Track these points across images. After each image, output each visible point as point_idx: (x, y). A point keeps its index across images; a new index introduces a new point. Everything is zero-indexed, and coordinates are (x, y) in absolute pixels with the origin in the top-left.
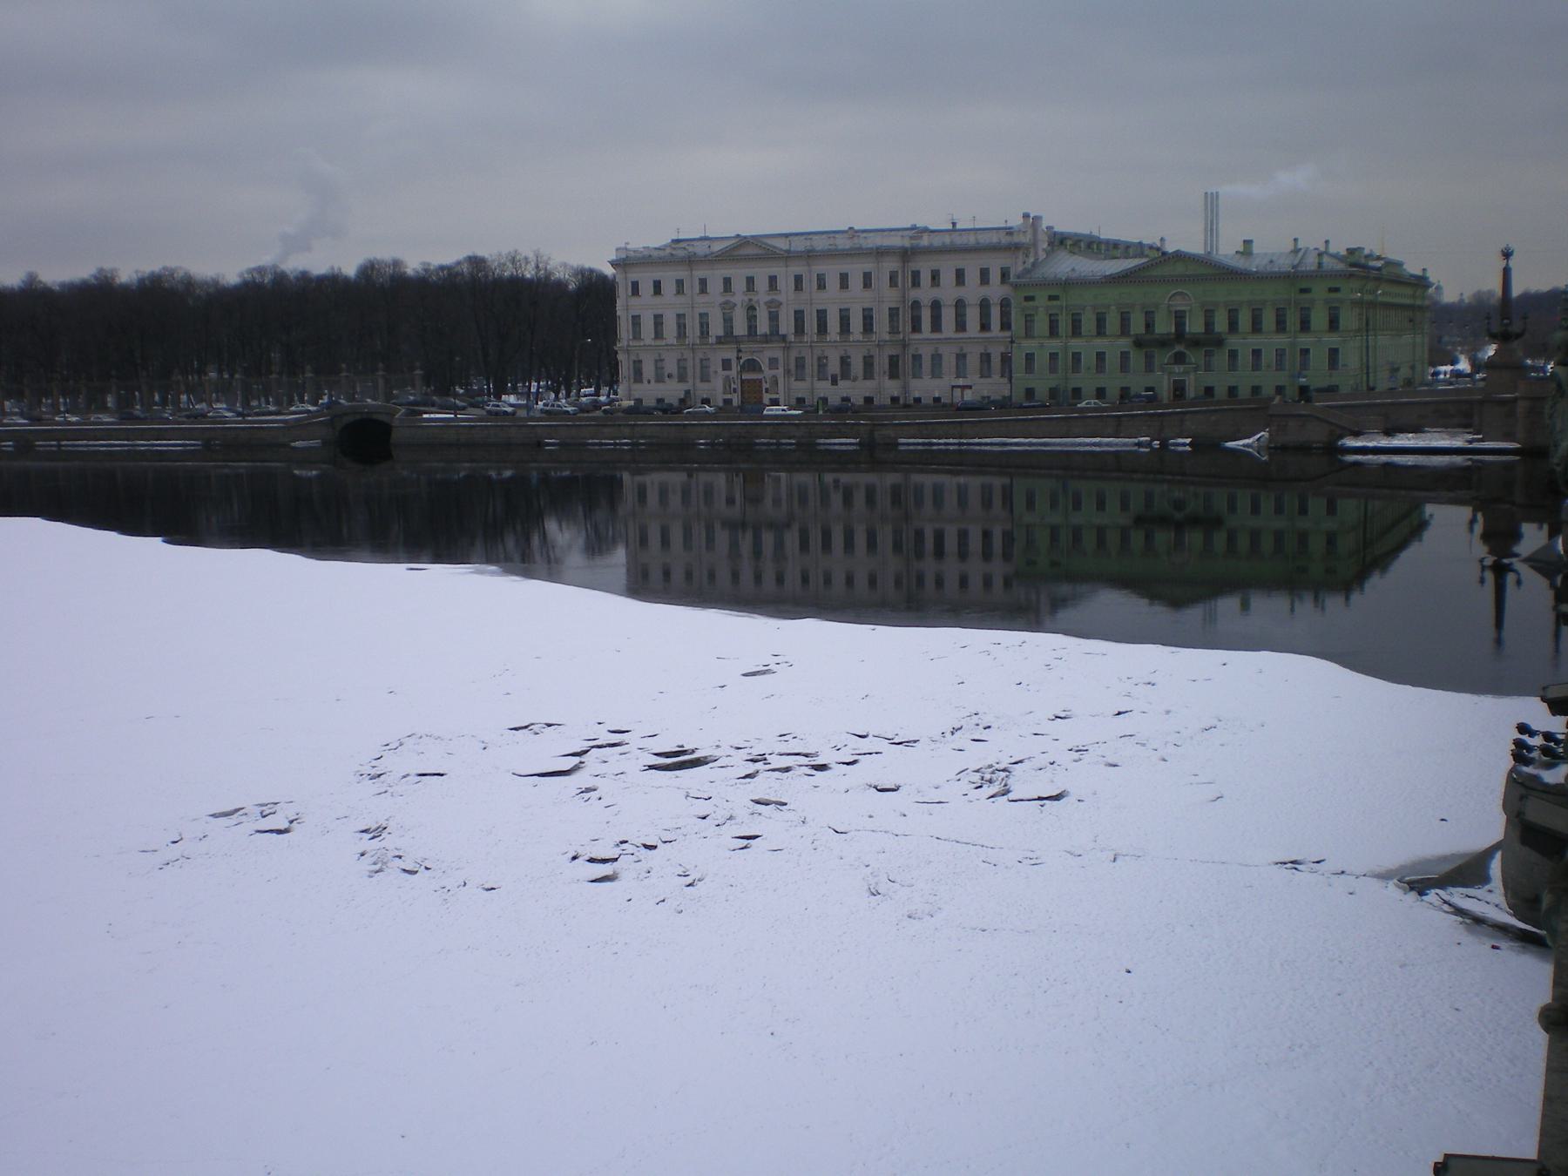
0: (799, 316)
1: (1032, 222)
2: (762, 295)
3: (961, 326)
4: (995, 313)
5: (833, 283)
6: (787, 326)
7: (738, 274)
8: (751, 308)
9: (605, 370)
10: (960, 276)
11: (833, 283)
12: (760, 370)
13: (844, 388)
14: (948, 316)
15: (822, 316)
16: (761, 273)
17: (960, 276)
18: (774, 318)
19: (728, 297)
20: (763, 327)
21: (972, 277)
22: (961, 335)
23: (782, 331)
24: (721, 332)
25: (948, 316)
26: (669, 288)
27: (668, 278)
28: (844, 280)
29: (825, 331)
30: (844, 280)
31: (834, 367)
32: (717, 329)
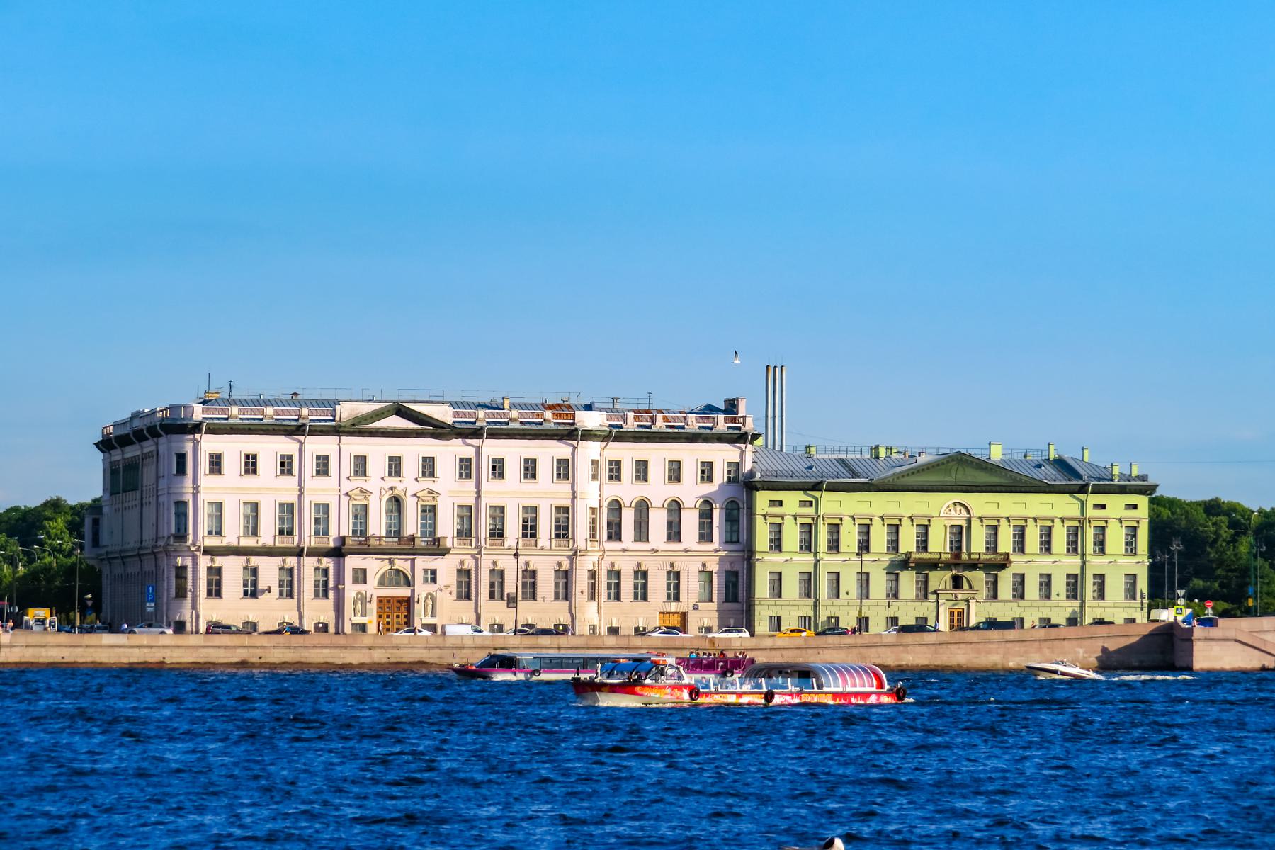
3: (674, 533)
5: (513, 469)
10: (675, 473)
11: (513, 469)
12: (409, 583)
13: (529, 613)
14: (658, 520)
16: (412, 450)
17: (675, 473)
18: (429, 512)
20: (412, 526)
21: (690, 472)
25: (658, 520)
27: (269, 448)
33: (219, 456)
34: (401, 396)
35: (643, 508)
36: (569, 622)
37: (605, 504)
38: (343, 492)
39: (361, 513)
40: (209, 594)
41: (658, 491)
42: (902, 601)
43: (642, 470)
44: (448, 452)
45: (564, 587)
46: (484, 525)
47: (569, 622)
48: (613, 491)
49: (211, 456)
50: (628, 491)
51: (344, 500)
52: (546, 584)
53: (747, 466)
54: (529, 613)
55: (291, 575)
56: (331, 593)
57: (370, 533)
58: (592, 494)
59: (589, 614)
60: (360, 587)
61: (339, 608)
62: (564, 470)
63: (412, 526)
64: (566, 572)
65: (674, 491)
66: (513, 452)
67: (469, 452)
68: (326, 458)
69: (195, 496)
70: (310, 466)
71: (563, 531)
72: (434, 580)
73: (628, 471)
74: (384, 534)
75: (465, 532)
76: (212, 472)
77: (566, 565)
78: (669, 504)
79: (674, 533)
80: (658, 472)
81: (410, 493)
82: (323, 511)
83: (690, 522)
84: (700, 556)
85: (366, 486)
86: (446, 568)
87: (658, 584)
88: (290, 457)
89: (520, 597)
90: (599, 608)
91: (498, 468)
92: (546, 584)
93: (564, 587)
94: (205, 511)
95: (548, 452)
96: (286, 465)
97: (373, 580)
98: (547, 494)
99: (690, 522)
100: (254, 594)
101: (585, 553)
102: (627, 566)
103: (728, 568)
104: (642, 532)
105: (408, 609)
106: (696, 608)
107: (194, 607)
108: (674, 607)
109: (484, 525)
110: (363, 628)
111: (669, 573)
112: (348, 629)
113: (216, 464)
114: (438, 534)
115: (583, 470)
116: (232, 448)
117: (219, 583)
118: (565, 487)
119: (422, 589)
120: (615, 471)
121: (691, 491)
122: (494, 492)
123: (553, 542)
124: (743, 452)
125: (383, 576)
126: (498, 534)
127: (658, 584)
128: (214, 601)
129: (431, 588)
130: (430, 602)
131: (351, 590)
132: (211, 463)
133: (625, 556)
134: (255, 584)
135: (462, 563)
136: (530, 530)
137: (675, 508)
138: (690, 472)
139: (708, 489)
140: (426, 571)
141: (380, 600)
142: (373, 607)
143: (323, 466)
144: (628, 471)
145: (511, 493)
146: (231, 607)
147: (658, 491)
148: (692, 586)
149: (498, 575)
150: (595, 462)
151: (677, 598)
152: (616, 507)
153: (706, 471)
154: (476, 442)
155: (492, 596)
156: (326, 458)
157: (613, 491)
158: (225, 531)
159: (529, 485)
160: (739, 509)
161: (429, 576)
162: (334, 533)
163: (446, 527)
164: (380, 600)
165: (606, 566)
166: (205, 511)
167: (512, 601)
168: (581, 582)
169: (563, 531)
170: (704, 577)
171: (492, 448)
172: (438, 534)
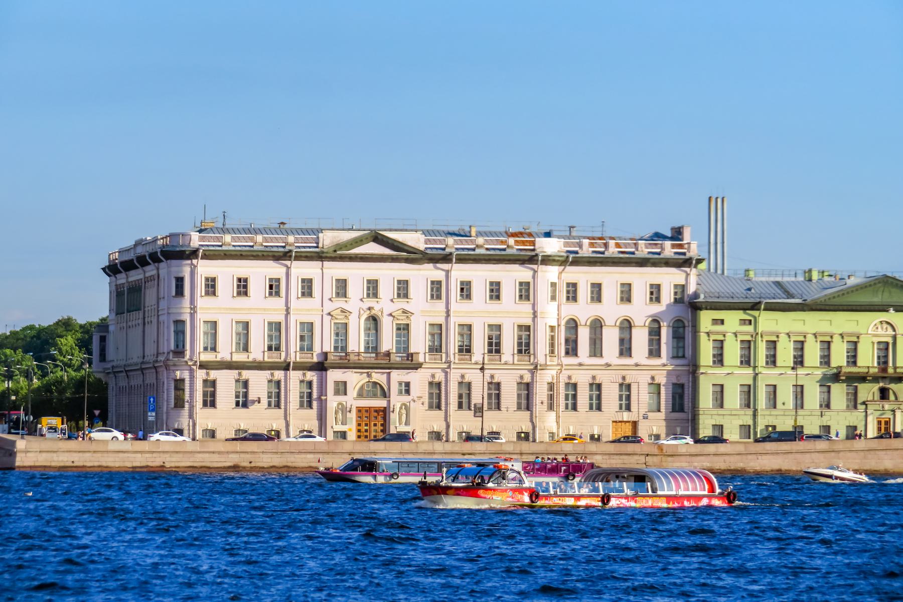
3: (626, 349)
5: (480, 291)
8: (374, 321)
10: (626, 295)
11: (480, 291)
12: (385, 395)
13: (492, 421)
14: (611, 338)
15: (467, 330)
16: (388, 274)
17: (626, 295)
18: (404, 330)
19: (371, 302)
20: (388, 342)
21: (640, 293)
25: (611, 338)
27: (260, 273)
31: (478, 395)
35: (597, 326)
36: (530, 430)
37: (563, 323)
38: (326, 312)
39: (342, 331)
40: (205, 404)
43: (597, 292)
44: (421, 276)
45: (526, 401)
46: (453, 342)
47: (530, 430)
48: (570, 310)
50: (584, 311)
51: (327, 319)
52: (509, 395)
53: (692, 289)
57: (350, 349)
58: (551, 314)
60: (341, 398)
62: (525, 292)
63: (388, 342)
64: (528, 384)
65: (626, 310)
70: (296, 288)
71: (525, 347)
72: (408, 392)
73: (584, 292)
74: (362, 350)
75: (436, 349)
76: (207, 293)
77: (527, 378)
78: (622, 323)
79: (626, 349)
80: (610, 293)
81: (386, 312)
82: (308, 328)
83: (640, 339)
86: (419, 380)
87: (611, 395)
90: (558, 417)
91: (466, 290)
92: (509, 395)
93: (526, 401)
94: (201, 329)
95: (511, 276)
96: (274, 288)
97: (352, 392)
98: (510, 314)
100: (245, 405)
101: (545, 367)
102: (582, 379)
103: (675, 381)
104: (596, 349)
105: (384, 418)
108: (626, 416)
109: (453, 342)
111: (621, 385)
113: (211, 286)
114: (412, 350)
115: (542, 292)
116: (225, 272)
118: (526, 307)
119: (397, 401)
120: (572, 293)
121: (641, 311)
122: (461, 311)
123: (516, 357)
124: (688, 275)
125: (362, 387)
126: (466, 349)
127: (611, 395)
128: (209, 411)
129: (405, 399)
130: (404, 411)
132: (207, 286)
133: (582, 370)
134: (246, 395)
135: (433, 376)
136: (495, 347)
138: (640, 293)
140: (400, 384)
141: (359, 410)
142: (353, 416)
144: (584, 292)
145: (478, 313)
147: (611, 310)
148: (642, 397)
149: (466, 386)
150: (553, 285)
151: (628, 408)
152: (573, 325)
153: (655, 293)
156: (310, 281)
157: (570, 310)
159: (494, 306)
160: (684, 327)
161: (403, 388)
162: (317, 349)
163: (419, 343)
164: (359, 410)
165: (563, 379)
166: (201, 329)
167: (479, 411)
168: (541, 393)
169: (525, 347)
171: (460, 272)
172: (412, 350)
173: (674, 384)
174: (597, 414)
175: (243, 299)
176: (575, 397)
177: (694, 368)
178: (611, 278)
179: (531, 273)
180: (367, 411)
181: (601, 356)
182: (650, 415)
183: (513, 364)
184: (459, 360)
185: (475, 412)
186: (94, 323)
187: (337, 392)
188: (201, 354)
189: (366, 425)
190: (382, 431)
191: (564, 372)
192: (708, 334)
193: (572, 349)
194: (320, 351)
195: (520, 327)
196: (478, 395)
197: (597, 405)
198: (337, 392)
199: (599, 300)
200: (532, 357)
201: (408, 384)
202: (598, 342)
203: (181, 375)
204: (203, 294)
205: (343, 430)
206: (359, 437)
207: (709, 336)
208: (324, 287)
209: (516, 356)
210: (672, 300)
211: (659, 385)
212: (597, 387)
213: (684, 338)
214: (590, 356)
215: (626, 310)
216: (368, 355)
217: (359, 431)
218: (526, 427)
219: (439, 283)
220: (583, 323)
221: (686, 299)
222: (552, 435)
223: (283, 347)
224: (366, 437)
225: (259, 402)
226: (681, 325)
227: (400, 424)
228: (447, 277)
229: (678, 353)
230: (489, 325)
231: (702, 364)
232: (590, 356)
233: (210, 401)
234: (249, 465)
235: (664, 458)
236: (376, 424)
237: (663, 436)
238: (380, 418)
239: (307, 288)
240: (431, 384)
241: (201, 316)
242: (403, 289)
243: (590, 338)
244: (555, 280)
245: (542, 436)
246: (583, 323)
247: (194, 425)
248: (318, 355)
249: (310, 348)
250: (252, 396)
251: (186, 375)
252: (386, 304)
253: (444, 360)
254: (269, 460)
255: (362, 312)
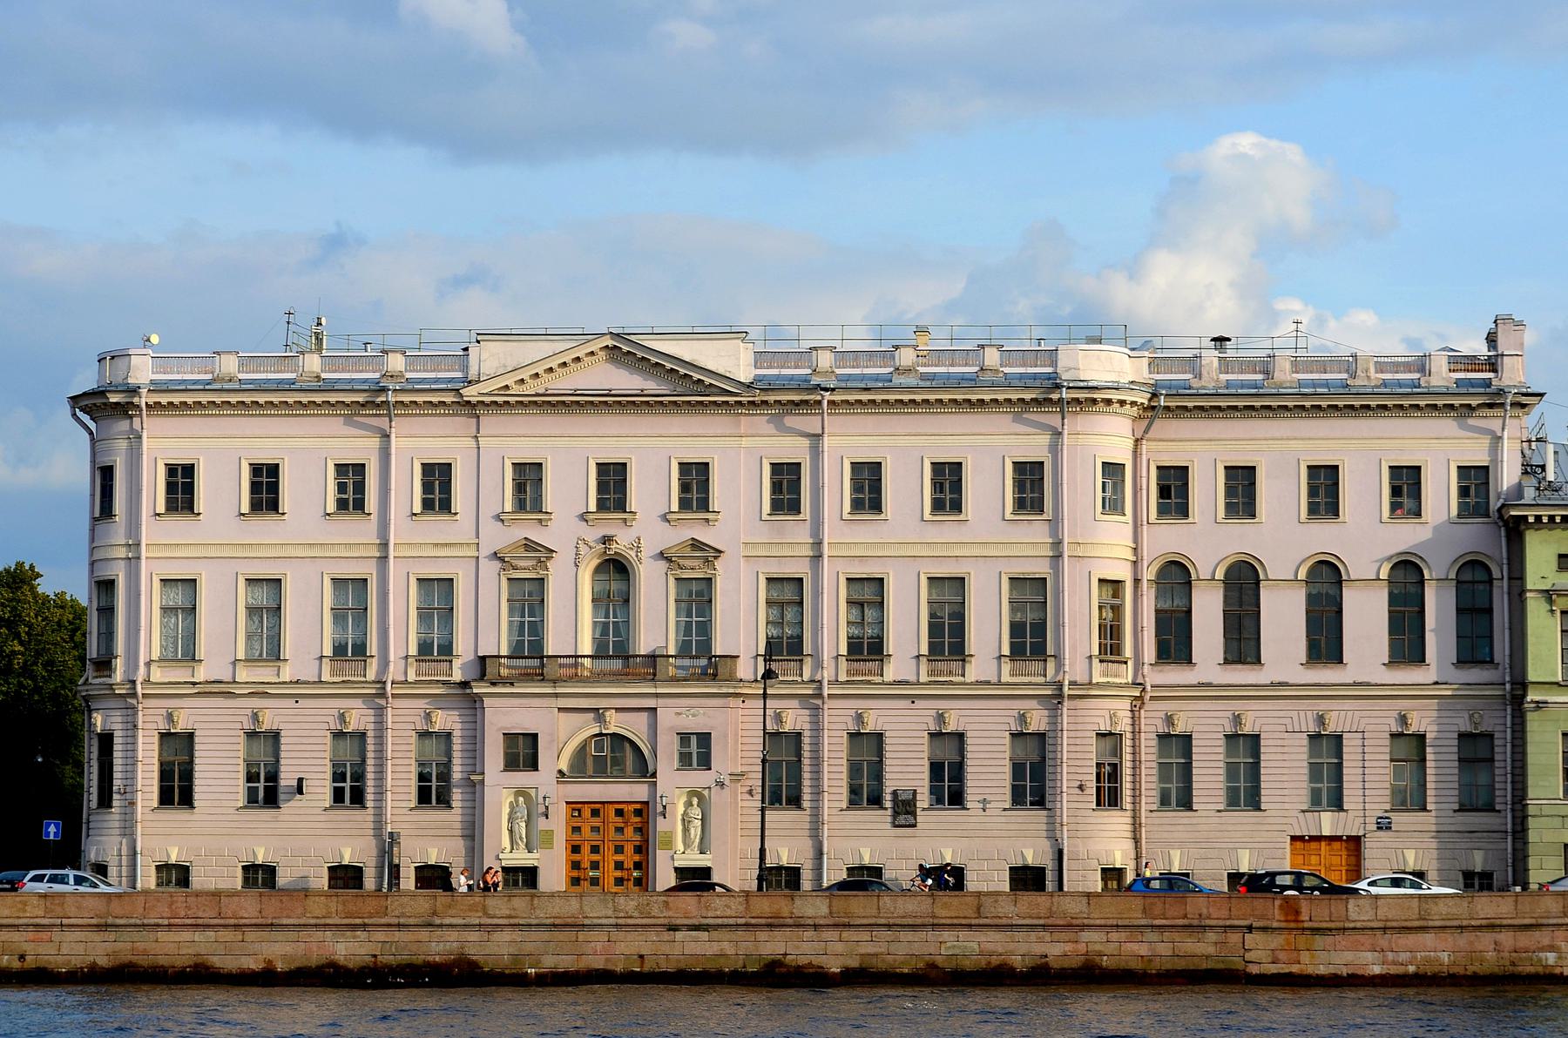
0: (787, 595)
1: (20, 565)
2: (649, 526)
3: (1325, 640)
4: (1438, 608)
5: (906, 489)
6: (740, 628)
7: (569, 455)
8: (616, 568)
9: (1043, 869)
10: (1324, 490)
11: (906, 489)
12: (645, 770)
13: (940, 838)
14: (1283, 617)
15: (868, 595)
16: (653, 451)
17: (1324, 490)
18: (697, 599)
19: (609, 525)
20: (655, 626)
21: (1364, 491)
22: (1326, 674)
23: (554, 644)
24: (496, 640)
25: (1283, 617)
26: (307, 490)
27: (309, 453)
28: (948, 485)
29: (958, 651)
30: (948, 485)
31: (907, 770)
32: (484, 627)
33: (189, 470)
34: (634, 318)
35: (1243, 582)
36: (1048, 862)
37: (1149, 574)
38: (485, 551)
39: (529, 600)
40: (166, 799)
41: (1282, 539)
42: (543, 895)
43: (1242, 488)
44: (741, 456)
45: (1032, 784)
46: (831, 628)
47: (1048, 862)
48: (1167, 539)
49: (172, 470)
50: (1207, 540)
51: (490, 569)
52: (989, 772)
53: (1508, 475)
54: (940, 838)
55: (1117, 751)
56: (457, 796)
57: (550, 650)
58: (1109, 547)
59: (1104, 841)
60: (522, 778)
61: (473, 833)
62: (1031, 486)
63: (655, 626)
64: (1041, 736)
65: (1324, 538)
66: (906, 449)
67: (791, 449)
68: (446, 469)
69: (133, 561)
70: (407, 489)
71: (1030, 639)
72: (705, 762)
73: (1207, 491)
74: (586, 648)
75: (785, 648)
76: (172, 507)
77: (1038, 721)
78: (1311, 571)
79: (1325, 640)
80: (1280, 493)
81: (649, 548)
82: (438, 595)
83: (1366, 617)
84: (1386, 691)
85: (537, 535)
86: (739, 734)
87: (1287, 771)
88: (360, 469)
89: (923, 800)
90: (1136, 826)
91: (868, 487)
92: (989, 772)
93: (1032, 784)
94: (152, 601)
95: (989, 449)
96: (351, 488)
97: (555, 757)
98: (989, 545)
99: (1366, 617)
100: (271, 799)
101: (1086, 691)
102: (1207, 727)
103: (1466, 726)
104: (1243, 640)
105: (642, 830)
106: (1384, 825)
107: (128, 830)
108: (1328, 823)
109: (831, 628)
110: (529, 876)
111: (1315, 738)
112: (665, 878)
113: (181, 487)
114: (718, 649)
115: (1077, 487)
116: (222, 453)
117: (188, 775)
118: (1034, 532)
119: (673, 784)
120: (1173, 489)
121: (1366, 538)
122: (850, 544)
123: (1006, 667)
124: (1497, 440)
125: (582, 750)
126: (867, 648)
127: (1287, 771)
128: (176, 816)
129: (699, 778)
130: (696, 812)
131: (500, 789)
132: (171, 487)
133: (1204, 695)
134: (273, 777)
135: (1022, 718)
136: (947, 638)
137: (1326, 585)
138: (1364, 491)
139: (1407, 536)
140: (684, 738)
141: (575, 807)
142: (558, 824)
143: (437, 485)
144: (1207, 491)
145: (904, 546)
146: (215, 837)
147: (1282, 539)
148: (1370, 776)
149: (868, 749)
150: (1112, 470)
151: (1337, 804)
152: (1176, 576)
153: (1406, 486)
154: (810, 423)
155: (855, 800)
156: (446, 469)
157: (1167, 539)
158: (288, 650)
159: (947, 530)
160: (1490, 581)
161: (694, 748)
162: (464, 649)
163: (740, 628)
164: (575, 807)
165: (1152, 722)
166: (152, 601)
167: (904, 809)
168: (1076, 764)
169: (1030, 639)
170: (1405, 749)
171: (847, 441)
172: (718, 649)
173: (1462, 736)
174: (1247, 817)
175: (265, 523)
176: (1187, 770)
177: (1516, 695)
178: (1281, 453)
179: (1044, 439)
180: (638, 813)
181: (1258, 661)
182: (1396, 818)
183: (918, 683)
184: (931, 673)
185: (896, 814)
186: (1225, 597)
187: (512, 764)
188: (153, 667)
189: (595, 849)
190: (638, 866)
191: (1149, 705)
192: (1548, 595)
193: (1174, 641)
194: (472, 657)
195: (338, 582)
196: (907, 770)
197: (1246, 792)
198: (512, 764)
199: (1333, 510)
200: (1051, 665)
201: (705, 739)
202: (1247, 622)
203: (104, 722)
204: (161, 508)
205: (529, 863)
206: (575, 881)
207: (1550, 601)
208: (482, 487)
209: (1096, 662)
210: (1454, 512)
211: (1421, 738)
212: (1178, 745)
213: (1490, 611)
214: (1227, 661)
215: (1240, 539)
216: (687, 662)
217: (576, 865)
218: (1034, 853)
219: (360, 469)
220: (1205, 573)
221: (1494, 505)
222: (1112, 874)
223: (373, 648)
224: (595, 882)
225: (300, 791)
226: (1480, 575)
227: (687, 844)
228: (816, 452)
229: (1473, 646)
230: (932, 580)
231: (1532, 676)
232: (1227, 661)
233: (177, 788)
234: (16, 964)
235: (1302, 940)
236: (618, 843)
237: (1432, 875)
238: (629, 832)
239: (437, 485)
240: (1231, 738)
241: (151, 572)
242: (695, 483)
243: (1227, 615)
244: (1123, 455)
245: (1083, 878)
246: (1205, 573)
247: (133, 854)
248: (463, 667)
249: (447, 649)
250: (287, 779)
251: (116, 724)
252: (649, 526)
253: (806, 678)
254: (80, 949)
255: (583, 549)
